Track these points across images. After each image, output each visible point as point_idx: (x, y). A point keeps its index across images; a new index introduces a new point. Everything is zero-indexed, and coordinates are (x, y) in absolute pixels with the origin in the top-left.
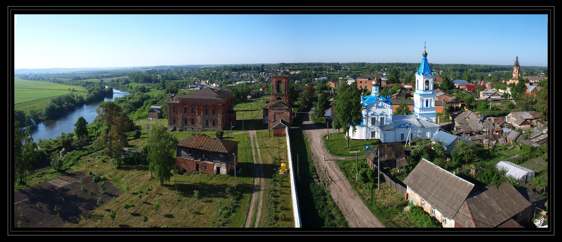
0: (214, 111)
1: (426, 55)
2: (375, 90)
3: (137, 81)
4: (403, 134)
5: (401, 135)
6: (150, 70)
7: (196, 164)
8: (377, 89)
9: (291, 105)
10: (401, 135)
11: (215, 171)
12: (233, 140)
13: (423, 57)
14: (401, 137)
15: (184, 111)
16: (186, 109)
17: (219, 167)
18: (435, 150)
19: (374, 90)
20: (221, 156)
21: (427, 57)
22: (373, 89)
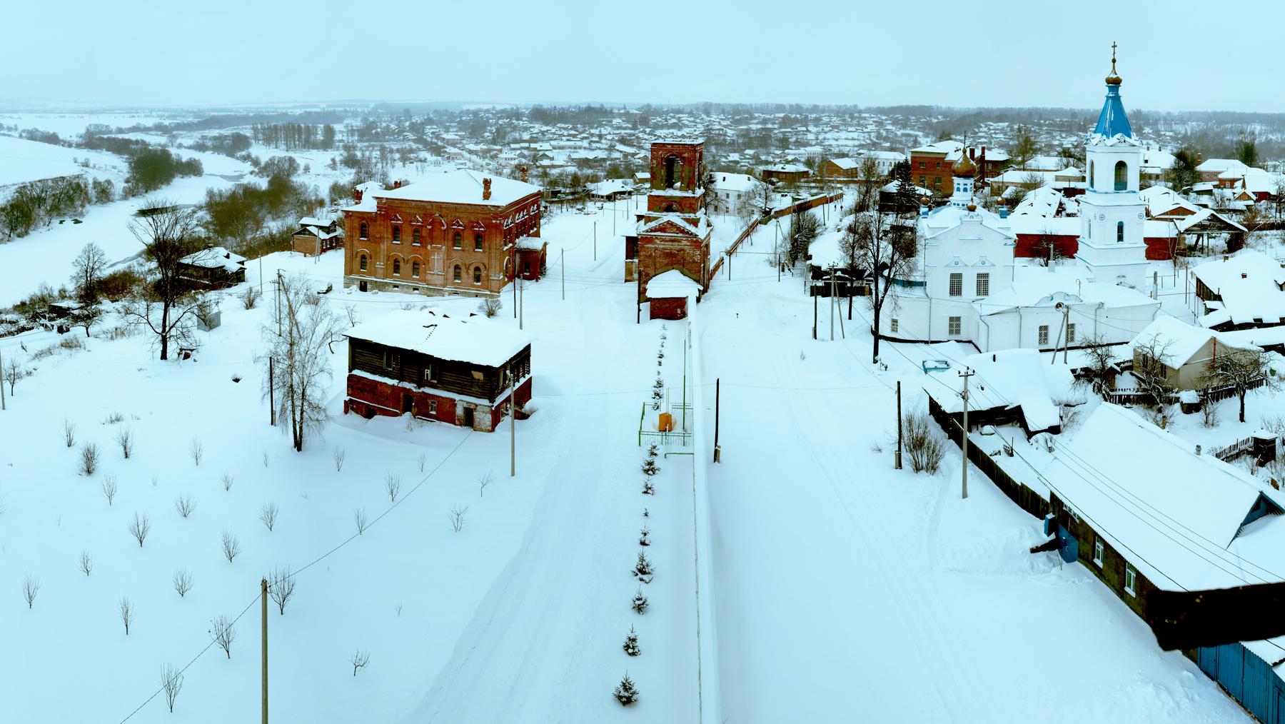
0: (480, 240)
1: (1114, 83)
2: (962, 190)
3: (234, 146)
4: (958, 319)
5: (951, 319)
6: (318, 110)
7: (404, 395)
8: (969, 187)
9: (903, 235)
10: (951, 319)
11: (459, 420)
12: (1011, 407)
13: (1105, 90)
14: (1040, 334)
15: (390, 236)
16: (399, 230)
17: (472, 407)
18: (158, 251)
19: (958, 189)
20: (478, 375)
21: (1121, 91)
22: (956, 186)
